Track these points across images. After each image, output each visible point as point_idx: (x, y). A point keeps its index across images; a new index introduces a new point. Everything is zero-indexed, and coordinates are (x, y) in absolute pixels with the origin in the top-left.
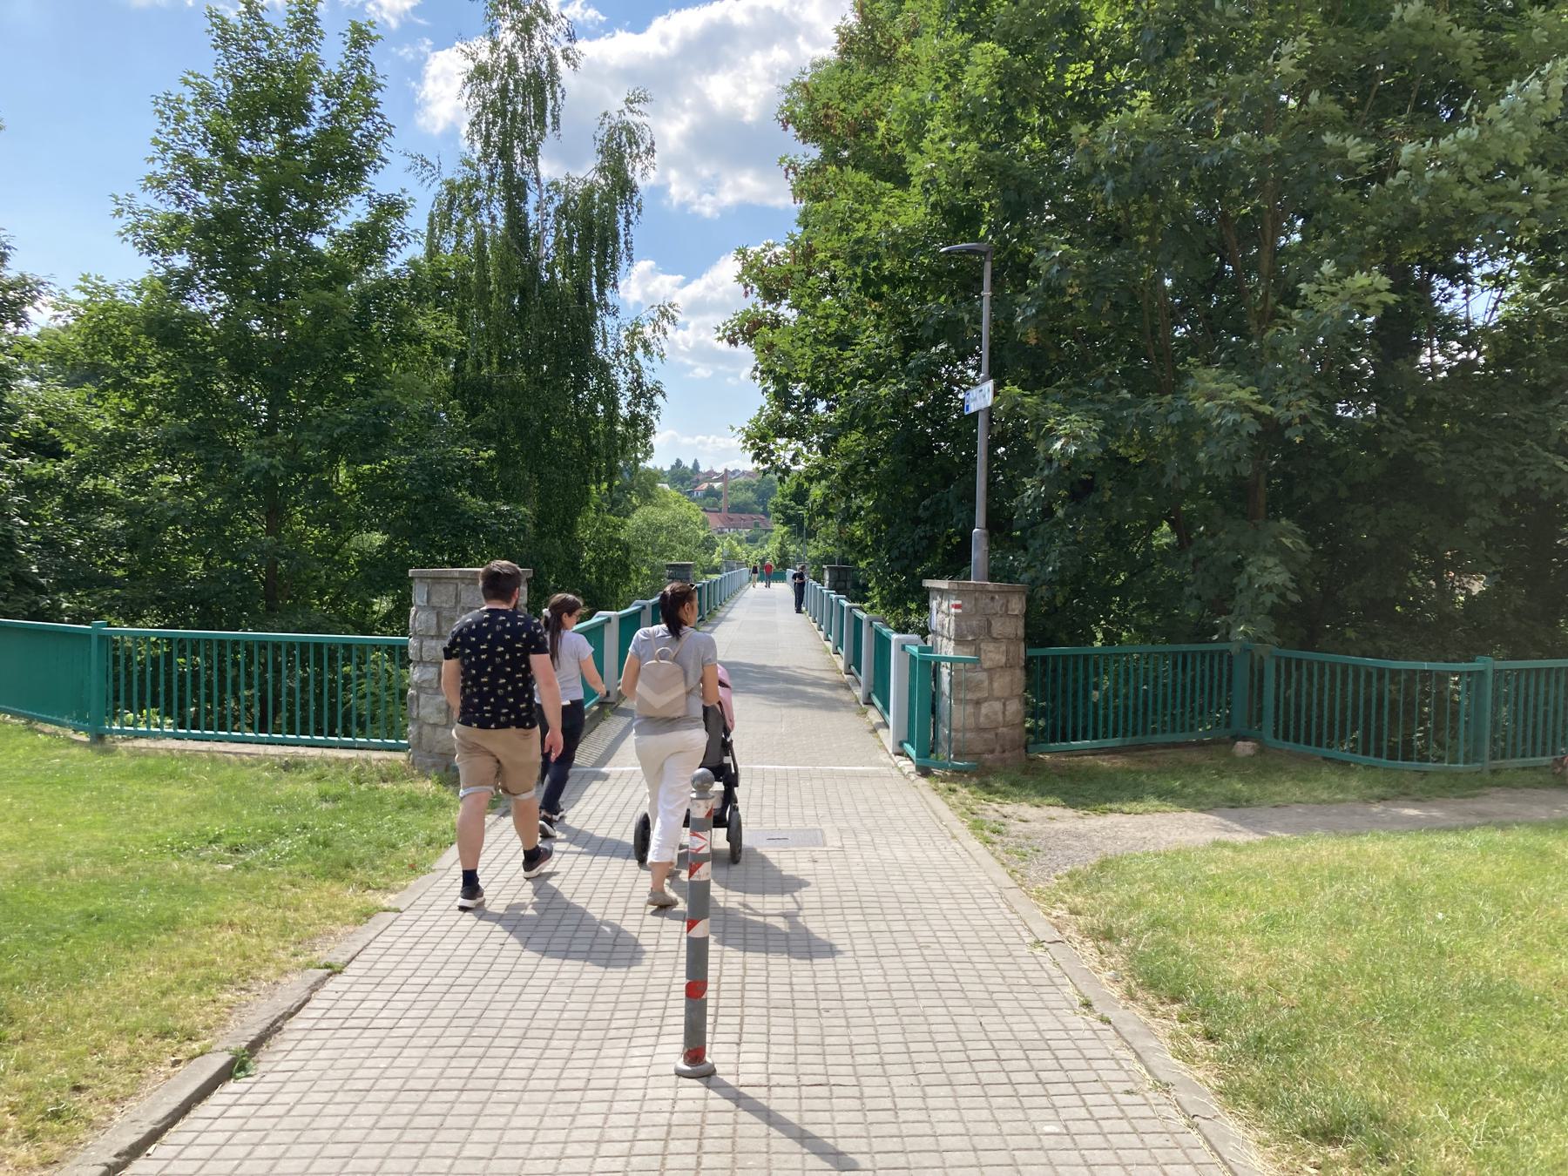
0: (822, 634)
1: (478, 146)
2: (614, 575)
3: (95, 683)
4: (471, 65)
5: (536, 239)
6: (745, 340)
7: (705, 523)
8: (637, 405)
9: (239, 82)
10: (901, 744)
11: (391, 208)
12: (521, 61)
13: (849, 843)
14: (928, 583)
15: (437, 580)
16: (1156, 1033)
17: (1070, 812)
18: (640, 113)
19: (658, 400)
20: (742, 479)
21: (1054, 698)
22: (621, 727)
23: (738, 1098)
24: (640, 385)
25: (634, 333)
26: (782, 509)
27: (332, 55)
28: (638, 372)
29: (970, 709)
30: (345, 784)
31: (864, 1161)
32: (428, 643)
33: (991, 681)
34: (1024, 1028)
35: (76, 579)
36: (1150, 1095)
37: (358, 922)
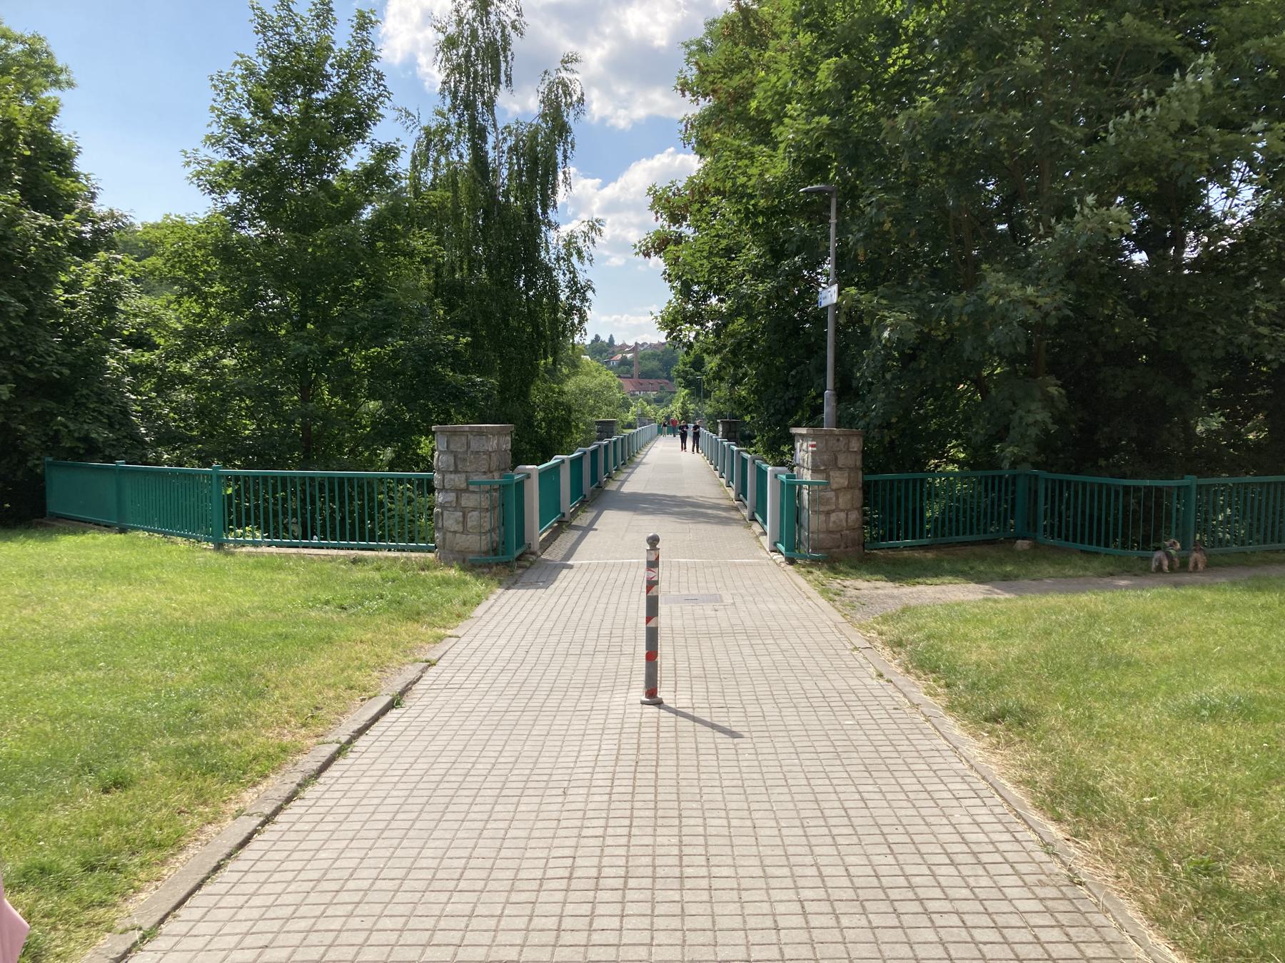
0: (717, 473)
1: (448, 101)
2: (560, 429)
3: (214, 510)
4: (442, 37)
5: (494, 171)
6: (656, 253)
7: (620, 387)
8: (574, 299)
9: (274, 59)
10: (775, 544)
11: (388, 153)
12: (480, 32)
13: (738, 600)
14: (794, 430)
15: (454, 433)
16: (917, 689)
17: (891, 584)
18: (573, 71)
19: (589, 294)
21: (883, 509)
22: (576, 537)
23: (676, 712)
24: (576, 283)
25: (569, 243)
27: (342, 38)
28: (573, 272)
29: (822, 517)
30: (396, 572)
31: (746, 734)
32: (448, 476)
33: (837, 498)
34: (840, 684)
35: (167, 438)
36: (908, 711)
37: (436, 642)
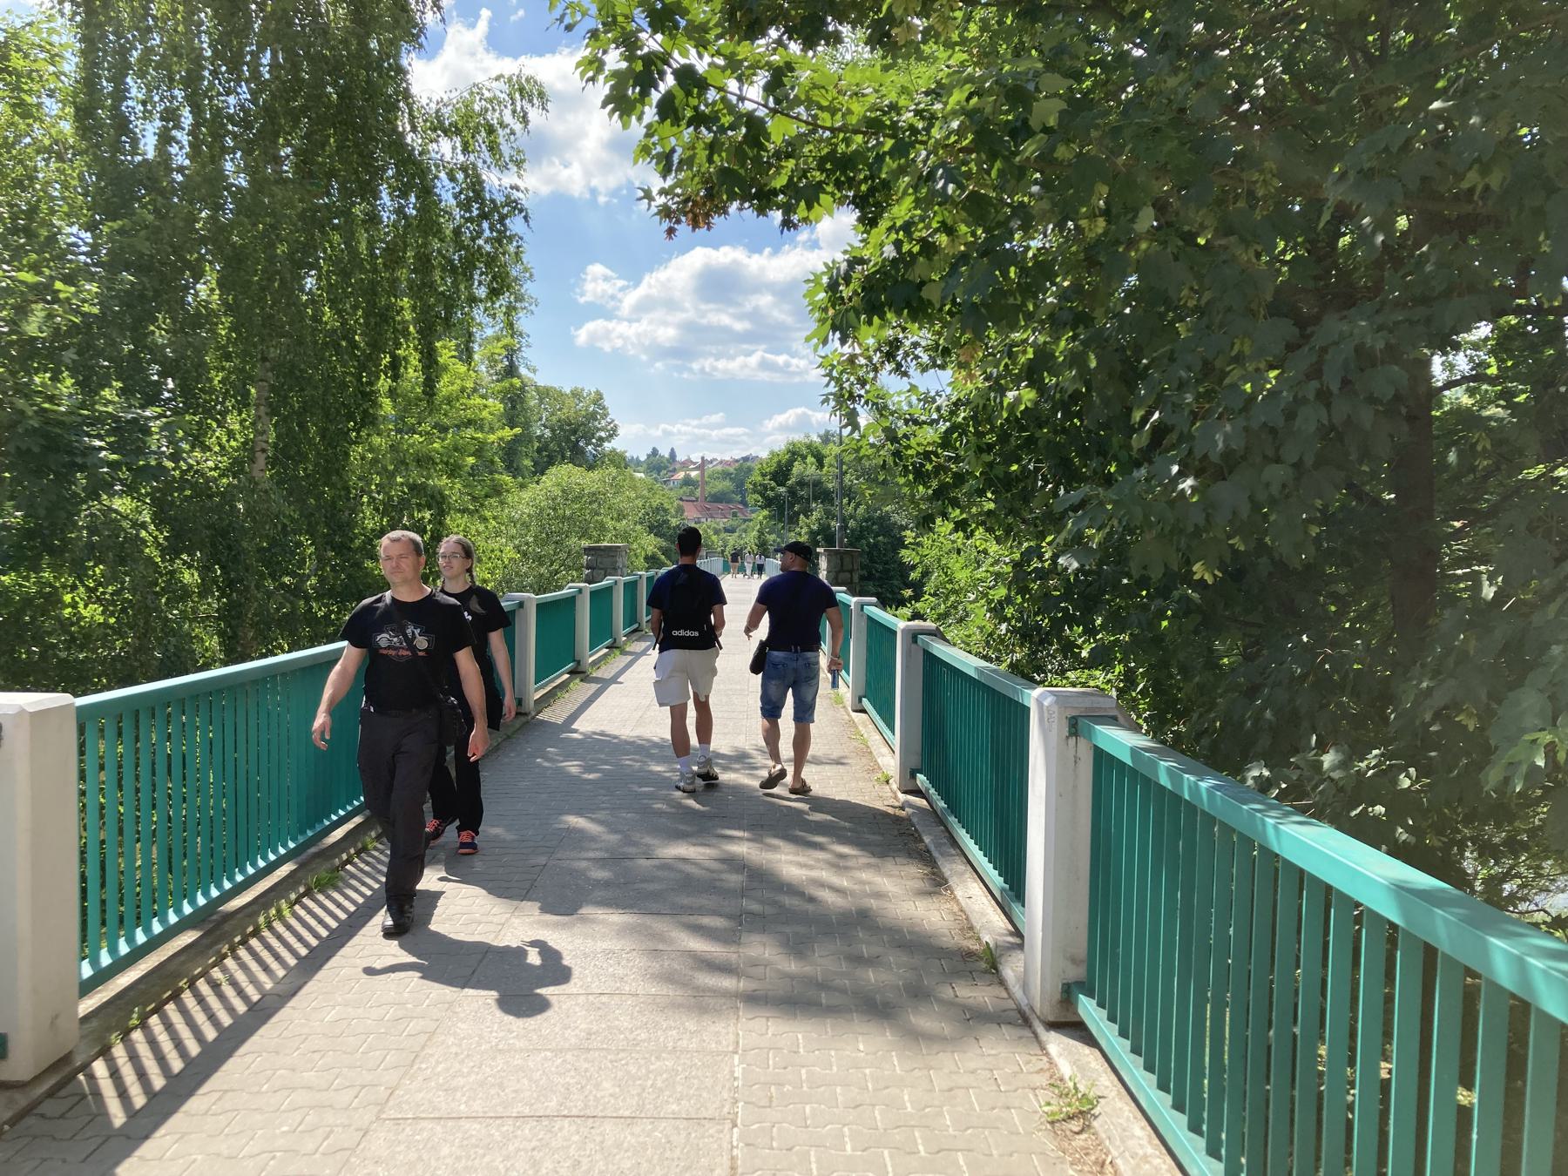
20: (719, 468)
26: (762, 490)
